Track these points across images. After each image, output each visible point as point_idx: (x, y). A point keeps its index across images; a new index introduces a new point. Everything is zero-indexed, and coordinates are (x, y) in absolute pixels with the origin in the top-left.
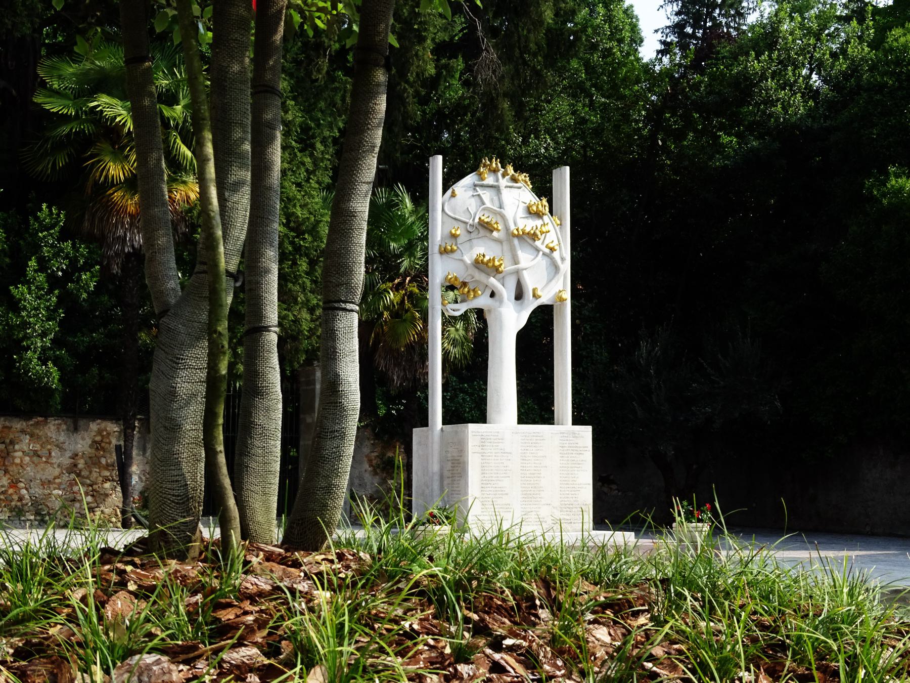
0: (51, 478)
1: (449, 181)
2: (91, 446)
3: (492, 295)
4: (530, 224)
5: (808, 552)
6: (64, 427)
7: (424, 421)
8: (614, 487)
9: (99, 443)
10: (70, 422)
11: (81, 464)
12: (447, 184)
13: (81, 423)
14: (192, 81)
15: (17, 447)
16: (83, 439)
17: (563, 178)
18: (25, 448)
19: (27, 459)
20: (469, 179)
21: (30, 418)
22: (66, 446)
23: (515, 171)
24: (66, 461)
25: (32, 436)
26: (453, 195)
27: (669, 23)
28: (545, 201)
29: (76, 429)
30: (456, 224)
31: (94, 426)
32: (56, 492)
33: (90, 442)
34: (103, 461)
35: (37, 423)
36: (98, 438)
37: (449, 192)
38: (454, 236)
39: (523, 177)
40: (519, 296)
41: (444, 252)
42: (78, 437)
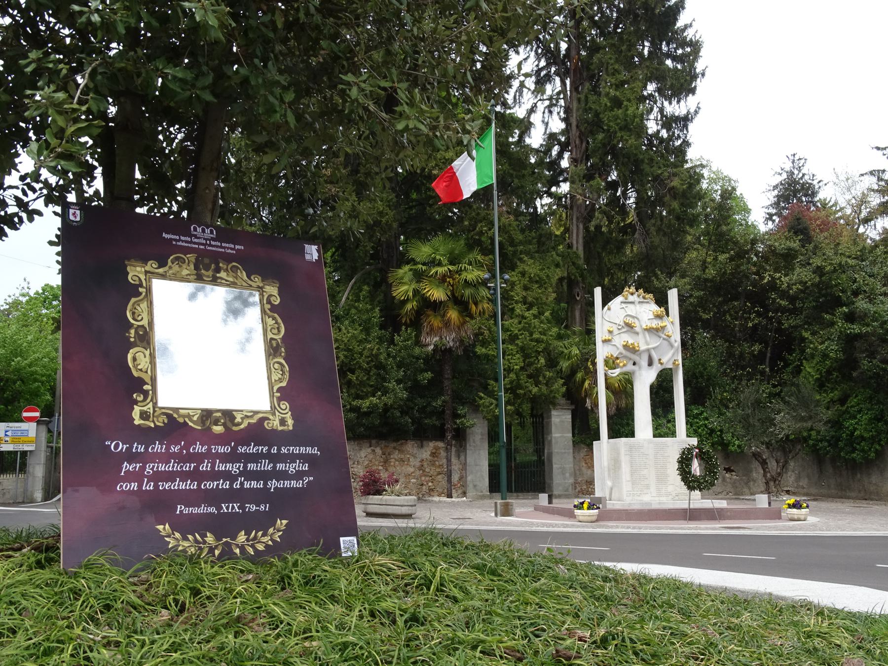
0: (410, 473)
1: (605, 301)
2: (430, 455)
3: (634, 364)
4: (655, 324)
5: (692, 507)
6: (416, 445)
7: (598, 438)
8: (734, 473)
9: (434, 453)
10: (419, 442)
11: (425, 464)
12: (605, 303)
13: (425, 443)
14: (76, 222)
15: (392, 456)
16: (426, 451)
17: (673, 296)
18: (396, 457)
19: (397, 463)
20: (620, 299)
21: (398, 441)
22: (417, 455)
23: (644, 292)
24: (418, 464)
25: (399, 450)
26: (609, 309)
27: (770, 203)
28: (662, 309)
29: (422, 446)
30: (611, 325)
31: (432, 444)
32: (412, 480)
33: (429, 453)
34: (437, 463)
35: (402, 444)
36: (434, 451)
37: (606, 307)
38: (610, 332)
39: (651, 296)
40: (650, 363)
41: (605, 341)
42: (423, 450)
